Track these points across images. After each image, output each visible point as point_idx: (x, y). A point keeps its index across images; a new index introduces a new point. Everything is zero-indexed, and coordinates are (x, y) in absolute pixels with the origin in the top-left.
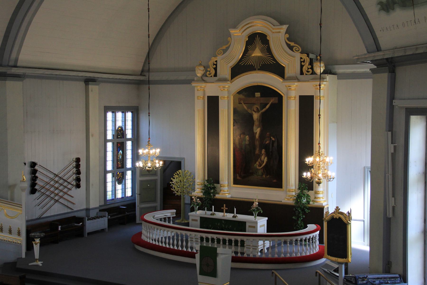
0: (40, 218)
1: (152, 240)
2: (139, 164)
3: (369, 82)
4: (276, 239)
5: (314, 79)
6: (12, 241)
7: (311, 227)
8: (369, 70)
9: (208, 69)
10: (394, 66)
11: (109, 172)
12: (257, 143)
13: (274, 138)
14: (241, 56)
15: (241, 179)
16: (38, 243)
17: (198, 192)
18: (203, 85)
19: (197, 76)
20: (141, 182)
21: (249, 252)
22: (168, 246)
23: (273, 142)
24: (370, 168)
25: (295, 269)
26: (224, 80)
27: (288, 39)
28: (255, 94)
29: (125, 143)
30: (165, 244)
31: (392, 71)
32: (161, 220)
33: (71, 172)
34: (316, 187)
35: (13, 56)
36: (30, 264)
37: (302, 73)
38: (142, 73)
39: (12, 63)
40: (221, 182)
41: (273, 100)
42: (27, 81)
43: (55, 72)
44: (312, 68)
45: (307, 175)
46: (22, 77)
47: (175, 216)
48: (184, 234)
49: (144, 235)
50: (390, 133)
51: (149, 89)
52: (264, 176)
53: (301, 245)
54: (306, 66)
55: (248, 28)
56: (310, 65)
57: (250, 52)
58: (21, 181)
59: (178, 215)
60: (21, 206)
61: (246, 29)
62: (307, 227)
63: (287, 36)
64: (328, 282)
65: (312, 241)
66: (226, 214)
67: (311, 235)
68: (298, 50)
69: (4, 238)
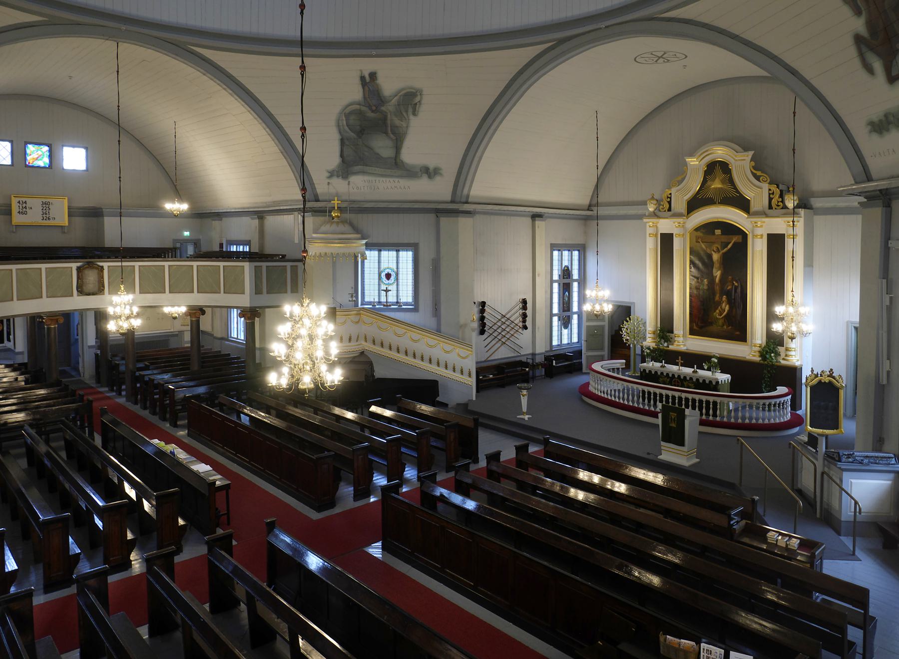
0: (485, 361)
1: (601, 392)
2: (587, 307)
3: (857, 220)
4: (741, 401)
5: (785, 215)
7: (782, 390)
8: (857, 203)
9: (662, 203)
10: (890, 199)
11: (555, 315)
12: (717, 288)
13: (737, 282)
14: (698, 188)
15: (698, 329)
17: (650, 342)
18: (655, 220)
19: (648, 210)
20: (588, 327)
21: (723, 416)
22: (622, 402)
23: (736, 288)
25: (772, 437)
26: (678, 215)
27: (753, 167)
28: (714, 231)
29: (571, 284)
30: (615, 397)
31: (888, 205)
32: (609, 370)
33: (518, 313)
34: (787, 343)
35: (465, 192)
36: (518, 417)
37: (770, 207)
38: (589, 208)
39: (464, 200)
40: (675, 332)
41: (735, 239)
42: (477, 217)
44: (783, 201)
45: (777, 327)
47: (624, 367)
48: (635, 388)
49: (592, 386)
50: (884, 281)
51: (598, 225)
52: (725, 327)
53: (769, 410)
54: (776, 198)
55: (706, 156)
56: (781, 197)
57: (709, 183)
58: (471, 321)
59: (628, 366)
61: (703, 158)
62: (777, 389)
63: (753, 164)
64: (804, 457)
65: (783, 406)
66: (681, 368)
67: (782, 400)
68: (766, 180)
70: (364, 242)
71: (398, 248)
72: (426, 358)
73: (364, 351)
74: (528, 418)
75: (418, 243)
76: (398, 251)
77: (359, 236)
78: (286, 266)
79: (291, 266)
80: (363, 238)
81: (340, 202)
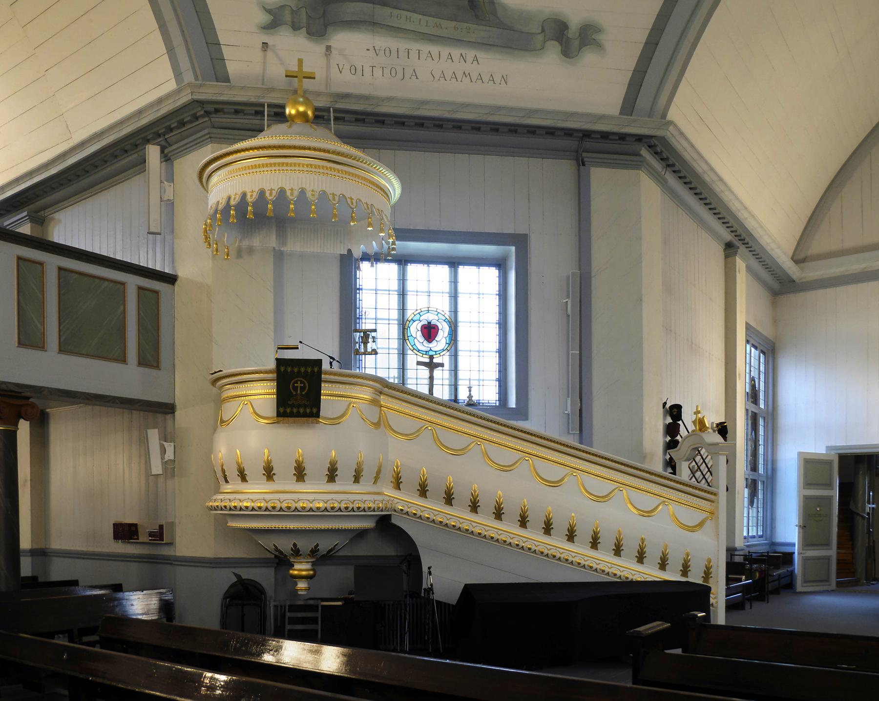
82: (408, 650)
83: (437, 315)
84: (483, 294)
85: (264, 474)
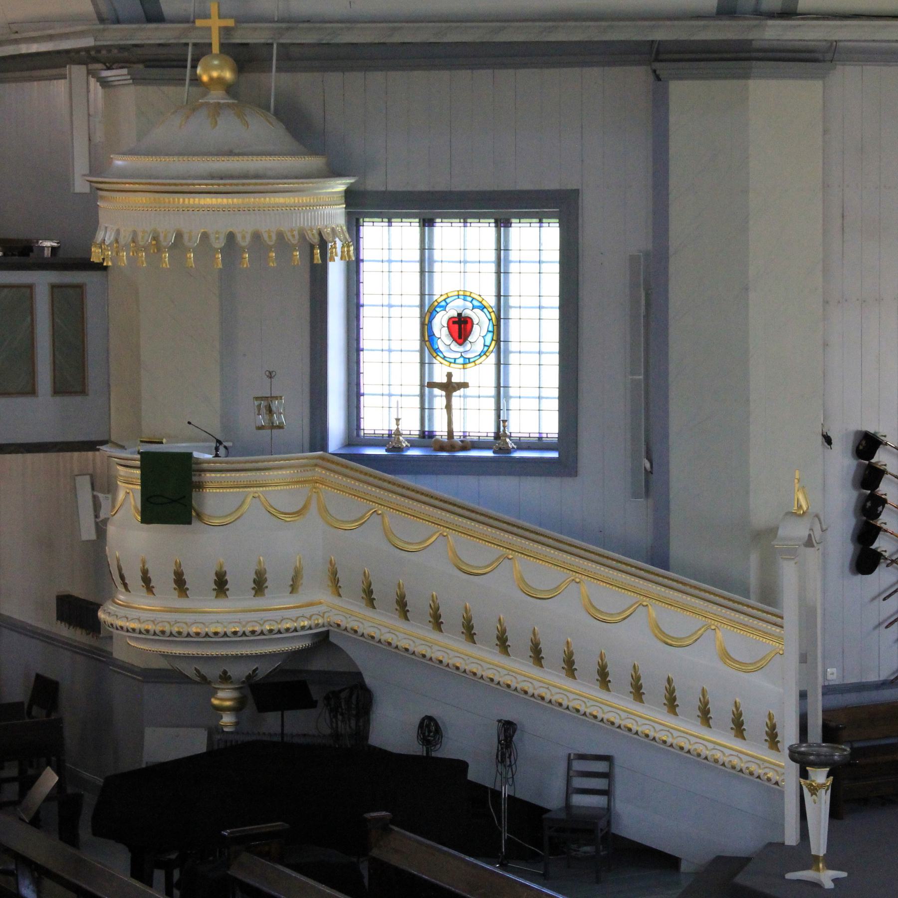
6: (743, 766)
16: (822, 786)
24: (139, 477)
36: (790, 876)
43: (841, 27)
46: (824, 61)
60: (778, 620)
69: (714, 752)
70: (339, 186)
71: (427, 212)
72: (586, 664)
73: (328, 632)
74: (835, 880)
75: (576, 192)
76: (502, 223)
77: (315, 162)
78: (30, 287)
79: (53, 287)
80: (334, 172)
81: (230, 23)
82: (277, 825)
83: (471, 302)
84: (383, 395)
85: (766, 740)
